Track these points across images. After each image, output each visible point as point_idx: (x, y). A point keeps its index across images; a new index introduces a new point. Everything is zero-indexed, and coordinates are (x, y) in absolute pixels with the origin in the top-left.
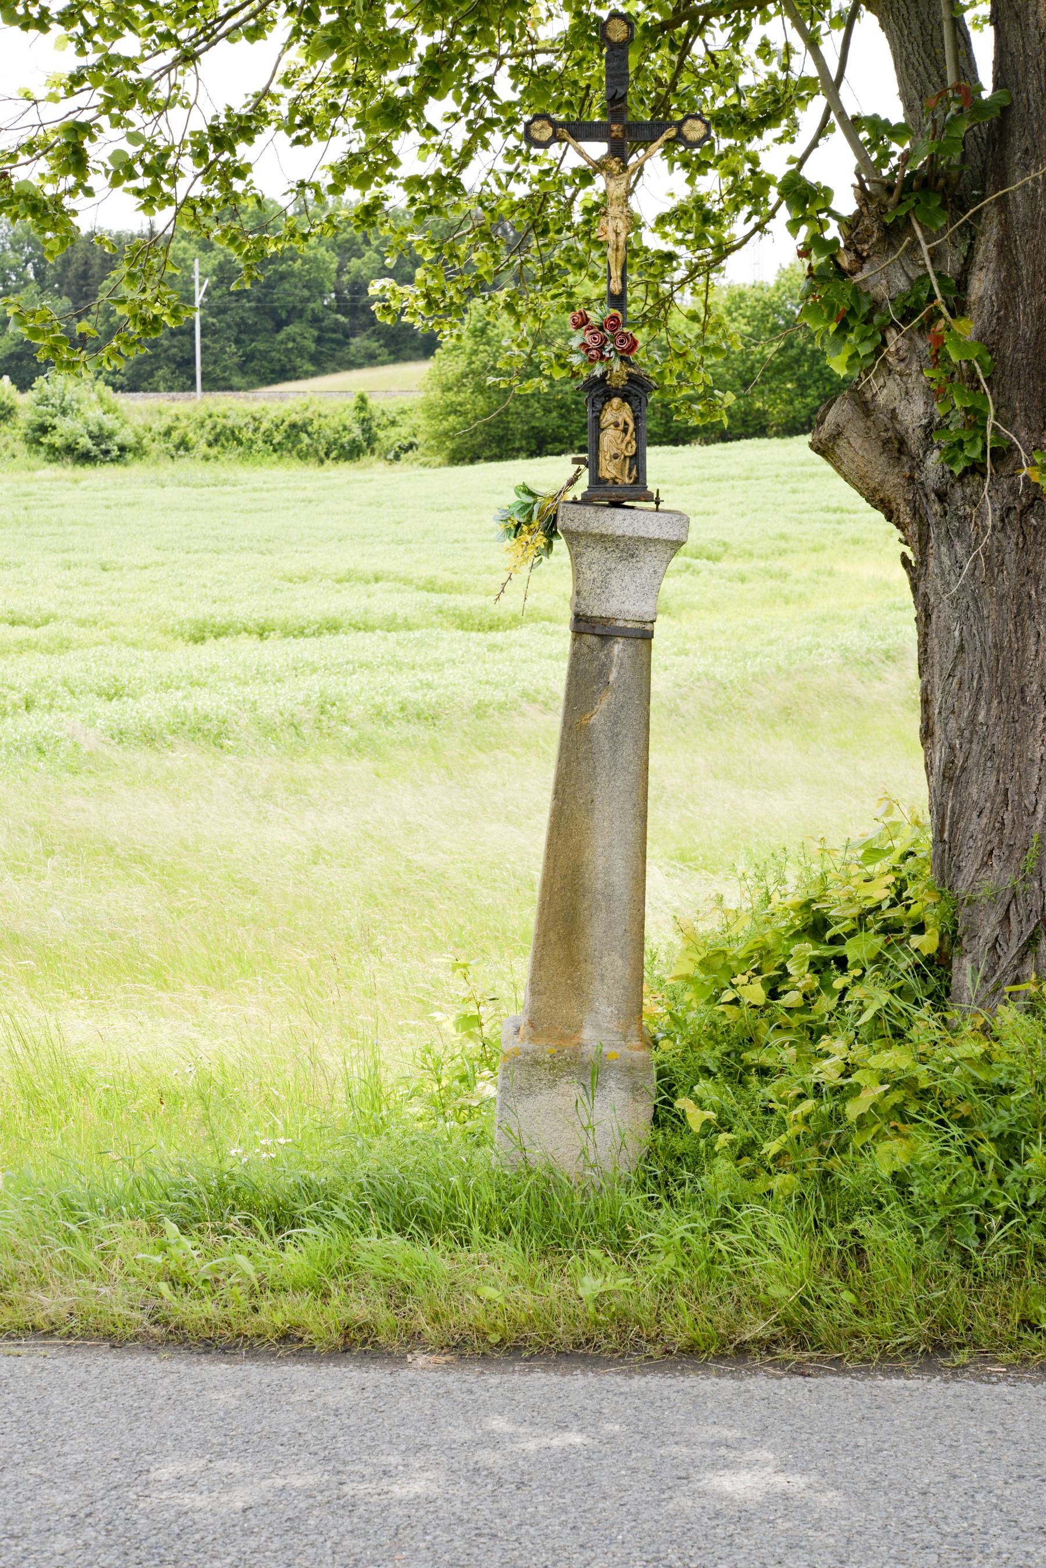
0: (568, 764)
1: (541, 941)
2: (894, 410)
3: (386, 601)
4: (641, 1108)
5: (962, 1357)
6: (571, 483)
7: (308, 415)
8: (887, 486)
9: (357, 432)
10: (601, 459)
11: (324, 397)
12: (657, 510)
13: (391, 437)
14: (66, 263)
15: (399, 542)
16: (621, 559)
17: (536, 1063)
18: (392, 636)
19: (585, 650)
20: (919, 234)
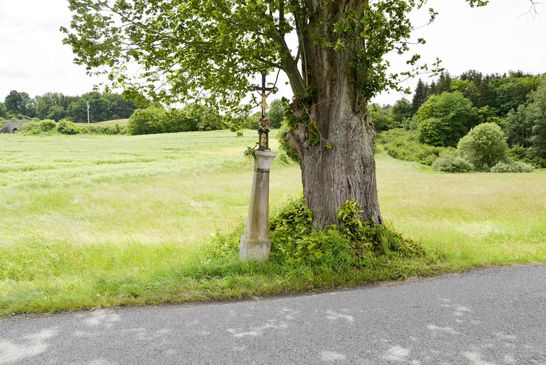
3: (129, 158)
5: (340, 287)
9: (116, 130)
11: (111, 124)
13: (122, 131)
14: (62, 101)
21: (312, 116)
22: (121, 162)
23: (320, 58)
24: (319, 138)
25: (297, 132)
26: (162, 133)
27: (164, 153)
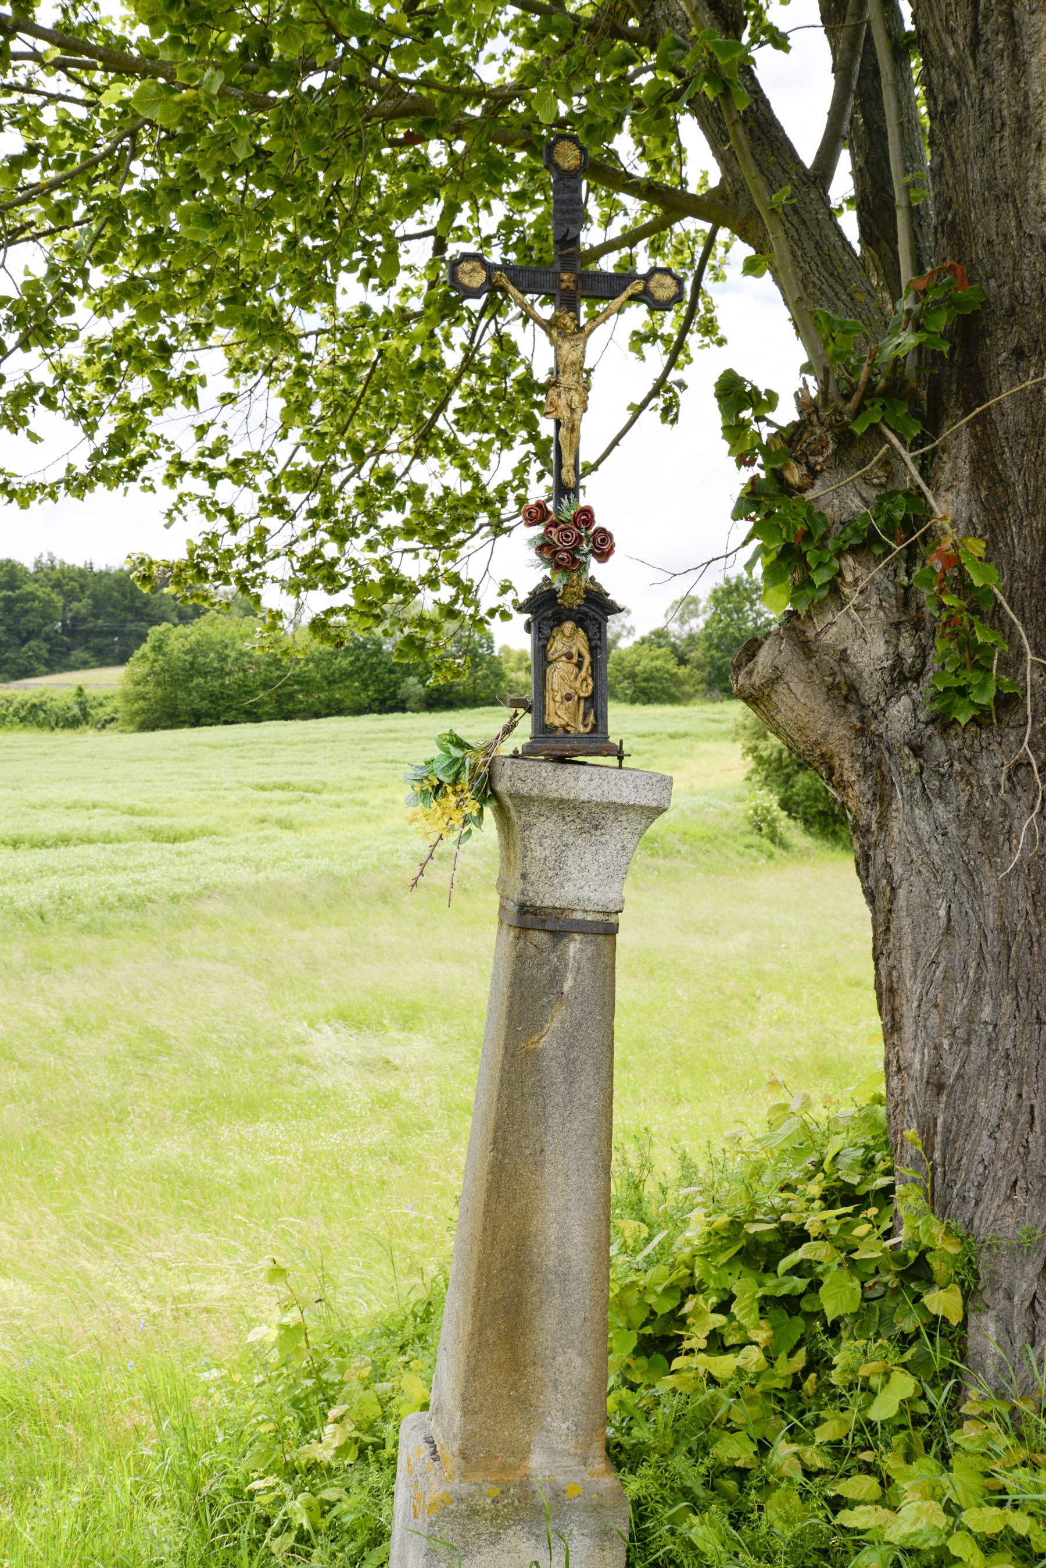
0: (510, 1103)
1: (475, 1343)
2: (845, 650)
3: (101, 823)
4: (608, 1555)
6: (508, 730)
7: (44, 699)
8: (831, 739)
9: (76, 710)
10: (549, 701)
11: (56, 687)
12: (620, 767)
13: (102, 713)
15: (109, 782)
16: (582, 831)
17: (474, 1512)
18: (109, 847)
19: (532, 951)
20: (895, 441)
21: (948, 507)
22: (65, 840)
23: (1002, 70)
24: (1012, 663)
25: (835, 628)
26: (257, 719)
27: (254, 802)
